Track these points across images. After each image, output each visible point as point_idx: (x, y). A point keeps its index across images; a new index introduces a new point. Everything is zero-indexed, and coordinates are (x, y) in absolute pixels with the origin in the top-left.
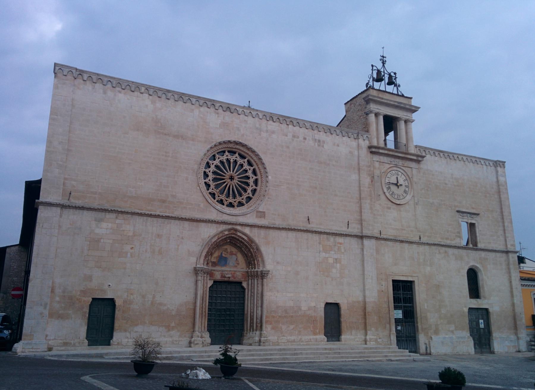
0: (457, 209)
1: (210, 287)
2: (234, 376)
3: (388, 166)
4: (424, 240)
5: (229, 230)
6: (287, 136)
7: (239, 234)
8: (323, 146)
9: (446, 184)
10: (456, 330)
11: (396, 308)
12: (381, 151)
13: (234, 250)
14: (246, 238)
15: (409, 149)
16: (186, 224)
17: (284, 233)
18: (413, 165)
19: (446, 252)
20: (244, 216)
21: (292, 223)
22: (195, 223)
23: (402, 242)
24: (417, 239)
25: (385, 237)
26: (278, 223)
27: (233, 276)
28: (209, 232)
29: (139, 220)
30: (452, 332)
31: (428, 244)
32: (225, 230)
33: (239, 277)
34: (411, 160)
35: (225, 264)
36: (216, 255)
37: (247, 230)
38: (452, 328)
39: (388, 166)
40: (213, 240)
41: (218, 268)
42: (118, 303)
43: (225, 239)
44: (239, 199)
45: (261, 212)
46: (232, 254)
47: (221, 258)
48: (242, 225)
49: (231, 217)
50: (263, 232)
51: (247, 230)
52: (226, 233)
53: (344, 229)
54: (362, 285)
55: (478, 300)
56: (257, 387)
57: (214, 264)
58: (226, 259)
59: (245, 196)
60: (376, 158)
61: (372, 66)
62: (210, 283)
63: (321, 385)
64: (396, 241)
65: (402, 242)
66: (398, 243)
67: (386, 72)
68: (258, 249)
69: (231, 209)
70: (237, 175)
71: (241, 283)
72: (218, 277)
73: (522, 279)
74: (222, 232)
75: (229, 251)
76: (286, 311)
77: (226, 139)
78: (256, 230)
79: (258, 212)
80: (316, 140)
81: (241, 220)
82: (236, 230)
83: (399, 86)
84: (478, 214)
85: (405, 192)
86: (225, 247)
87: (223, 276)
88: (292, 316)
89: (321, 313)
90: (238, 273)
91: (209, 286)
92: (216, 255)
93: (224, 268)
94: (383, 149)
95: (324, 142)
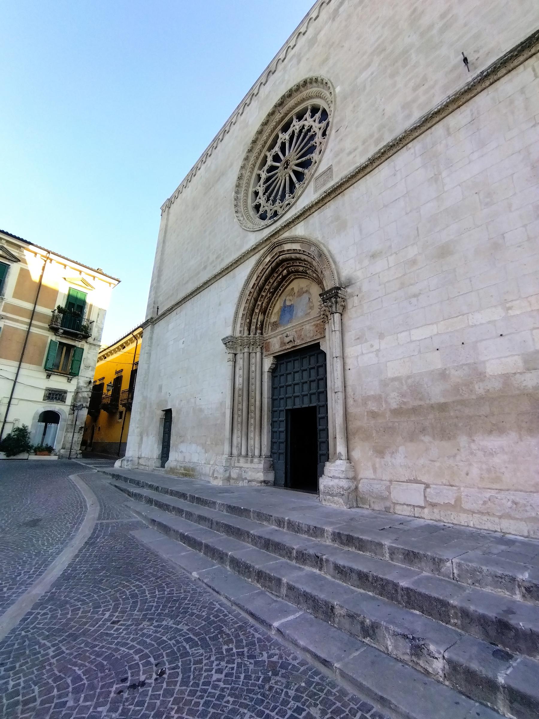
1: (273, 371)
7: (287, 247)
27: (300, 336)
32: (265, 256)
43: (273, 270)
46: (301, 293)
52: (268, 259)
62: (268, 363)
68: (321, 255)
71: (318, 345)
76: (416, 390)
87: (283, 344)
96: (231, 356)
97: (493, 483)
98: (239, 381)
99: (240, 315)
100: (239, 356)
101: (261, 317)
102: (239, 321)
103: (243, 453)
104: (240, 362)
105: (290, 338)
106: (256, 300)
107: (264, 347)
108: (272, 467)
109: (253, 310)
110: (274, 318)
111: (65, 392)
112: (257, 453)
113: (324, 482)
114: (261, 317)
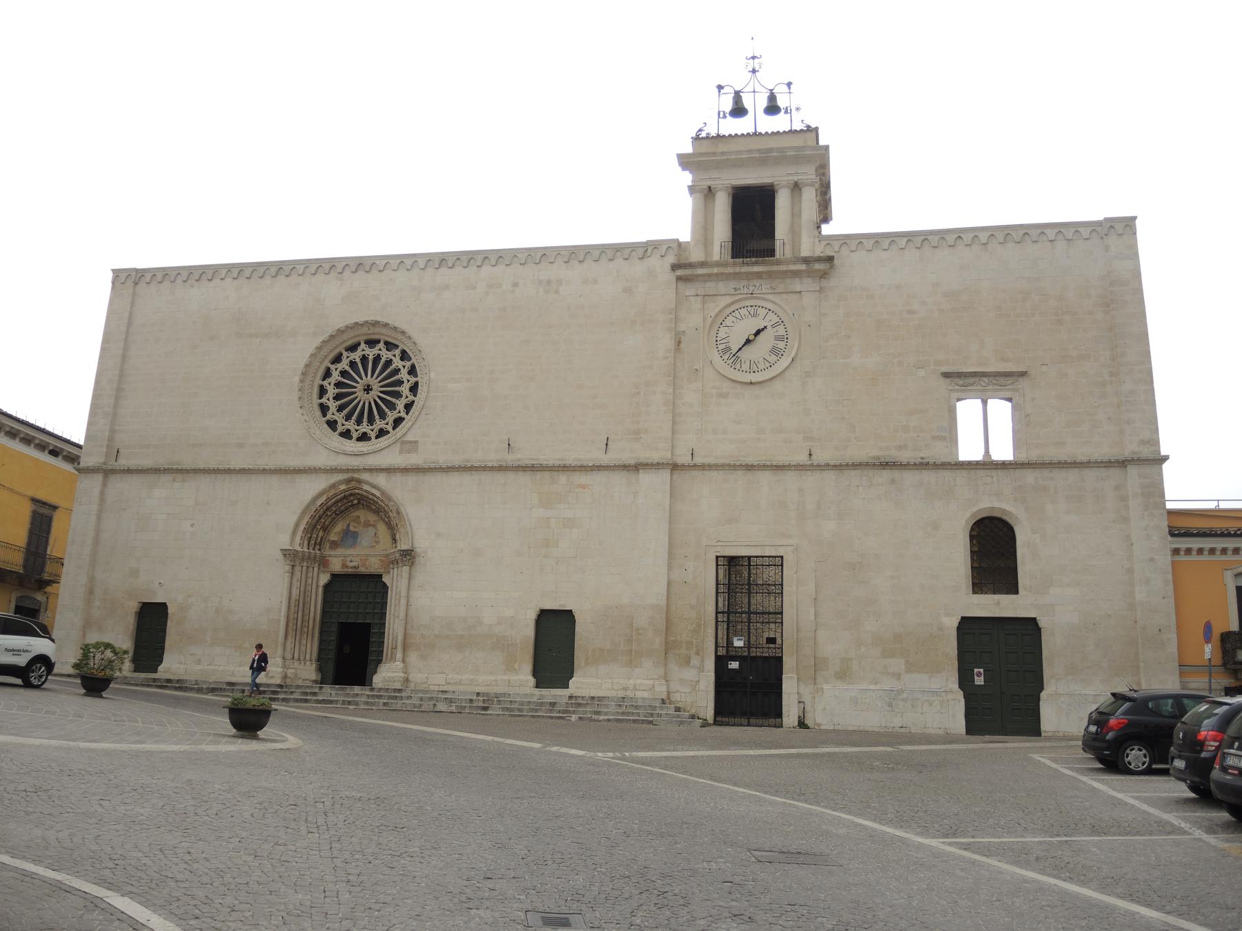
0: (945, 369)
1: (326, 587)
2: (104, 694)
3: (729, 300)
4: (821, 457)
5: (349, 481)
6: (474, 288)
7: (366, 487)
8: (557, 292)
9: (911, 312)
10: (908, 671)
12: (700, 271)
13: (372, 518)
14: (378, 494)
16: (275, 479)
17: (454, 478)
18: (807, 285)
19: (893, 481)
20: (333, 453)
21: (477, 458)
22: (289, 476)
23: (750, 468)
24: (802, 458)
25: (706, 461)
26: (443, 459)
28: (311, 489)
29: (204, 482)
30: (898, 676)
31: (839, 467)
32: (340, 483)
33: (373, 566)
34: (796, 274)
35: (353, 545)
37: (381, 480)
38: (898, 664)
39: (729, 300)
40: (319, 503)
41: (340, 551)
42: (171, 610)
43: (345, 497)
45: (410, 442)
46: (367, 524)
48: (370, 470)
49: (353, 458)
50: (411, 479)
51: (381, 480)
52: (343, 487)
53: (596, 455)
54: (634, 572)
56: (1196, 921)
58: (355, 535)
59: (339, 418)
60: (689, 290)
62: (324, 579)
64: (733, 467)
65: (750, 468)
66: (740, 473)
68: (398, 513)
71: (380, 576)
72: (336, 566)
73: (1174, 533)
74: (333, 486)
75: (362, 519)
77: (351, 321)
78: (398, 478)
79: (403, 443)
80: (540, 282)
81: (372, 461)
82: (359, 481)
84: (1023, 374)
85: (775, 351)
86: (357, 513)
87: (344, 566)
88: (462, 636)
89: (528, 631)
90: (373, 560)
92: (339, 527)
93: (348, 552)
94: (703, 264)
95: (560, 282)
96: (288, 568)
97: (1226, 695)
98: (295, 592)
99: (302, 528)
100: (298, 569)
101: (321, 534)
102: (299, 534)
103: (296, 656)
104: (297, 573)
105: (355, 564)
106: (320, 518)
107: (323, 563)
108: (320, 669)
109: (315, 526)
110: (333, 537)
111: (1013, 588)
112: (308, 657)
113: (378, 680)
114: (321, 534)
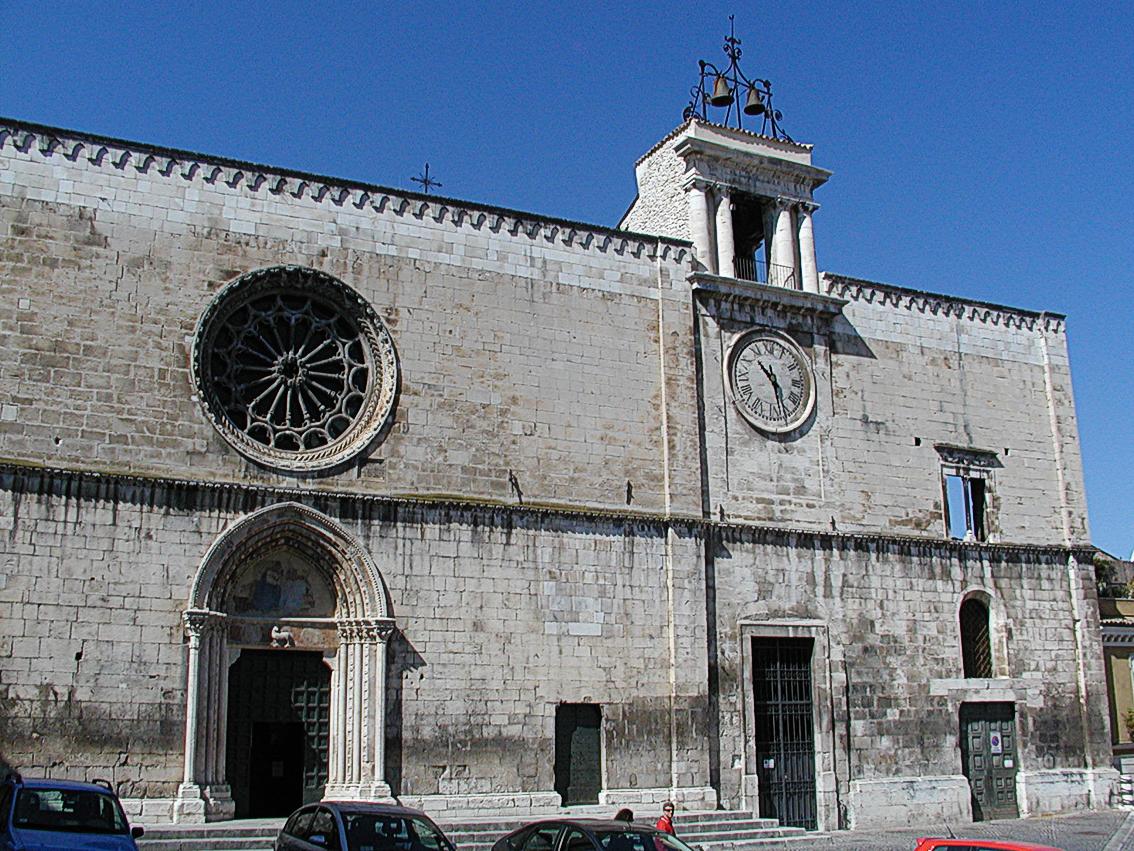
11: (461, 525)
15: (640, 762)
36: (248, 578)
44: (310, 426)
46: (292, 575)
47: (261, 586)
55: (818, 655)
57: (243, 606)
58: (276, 591)
61: (702, 64)
63: (740, 521)
67: (740, 79)
69: (290, 454)
70: (301, 357)
75: (284, 566)
83: (779, 116)
91: (227, 664)
